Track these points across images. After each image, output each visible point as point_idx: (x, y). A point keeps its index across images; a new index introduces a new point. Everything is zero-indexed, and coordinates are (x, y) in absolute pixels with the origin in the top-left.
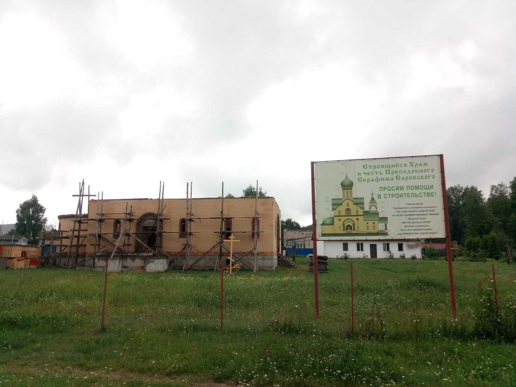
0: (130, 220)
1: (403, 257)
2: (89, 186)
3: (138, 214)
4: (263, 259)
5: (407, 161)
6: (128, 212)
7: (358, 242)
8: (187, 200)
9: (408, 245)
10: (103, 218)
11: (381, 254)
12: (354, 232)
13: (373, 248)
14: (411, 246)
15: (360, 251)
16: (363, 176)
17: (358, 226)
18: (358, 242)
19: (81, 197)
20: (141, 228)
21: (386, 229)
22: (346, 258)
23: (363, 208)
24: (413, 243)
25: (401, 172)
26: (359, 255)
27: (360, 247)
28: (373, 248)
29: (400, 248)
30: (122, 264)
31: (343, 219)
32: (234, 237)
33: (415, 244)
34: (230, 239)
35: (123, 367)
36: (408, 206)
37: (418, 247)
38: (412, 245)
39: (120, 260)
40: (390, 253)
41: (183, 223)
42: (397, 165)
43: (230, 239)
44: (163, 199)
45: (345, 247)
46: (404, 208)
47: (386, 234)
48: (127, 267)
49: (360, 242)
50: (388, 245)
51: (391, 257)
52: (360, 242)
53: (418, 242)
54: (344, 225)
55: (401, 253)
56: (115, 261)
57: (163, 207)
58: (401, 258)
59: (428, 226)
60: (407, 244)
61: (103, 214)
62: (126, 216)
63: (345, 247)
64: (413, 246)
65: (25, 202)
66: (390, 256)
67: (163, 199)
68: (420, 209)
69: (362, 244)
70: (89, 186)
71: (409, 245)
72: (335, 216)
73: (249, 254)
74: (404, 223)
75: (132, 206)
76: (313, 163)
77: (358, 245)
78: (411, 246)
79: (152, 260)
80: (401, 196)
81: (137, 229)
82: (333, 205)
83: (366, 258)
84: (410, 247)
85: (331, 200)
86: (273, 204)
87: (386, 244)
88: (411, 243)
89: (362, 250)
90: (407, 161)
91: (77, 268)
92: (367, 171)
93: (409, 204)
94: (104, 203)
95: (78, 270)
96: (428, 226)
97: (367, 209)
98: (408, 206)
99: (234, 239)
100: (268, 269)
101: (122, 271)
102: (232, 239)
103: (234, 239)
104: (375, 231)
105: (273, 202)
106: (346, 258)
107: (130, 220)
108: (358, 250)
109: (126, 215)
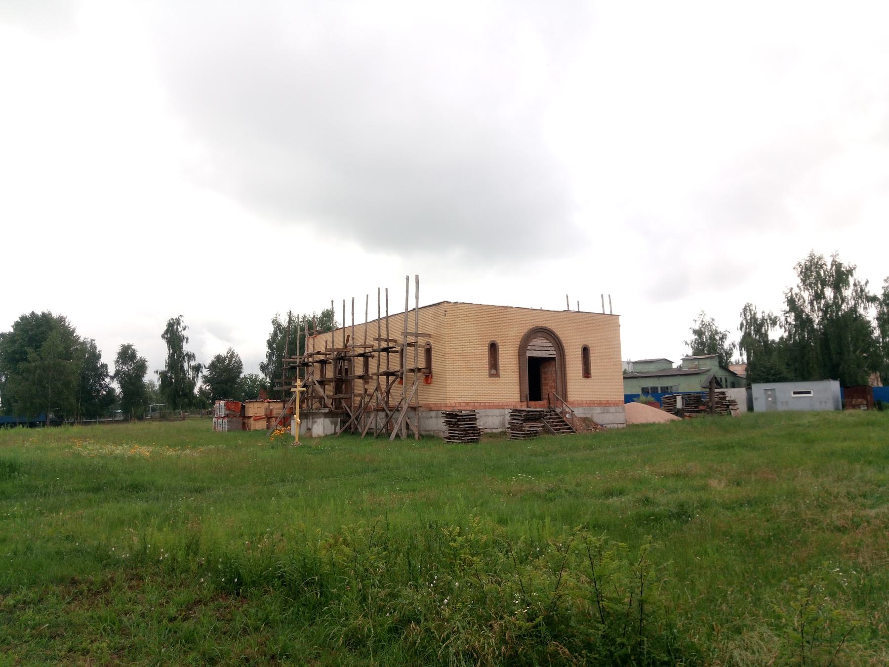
67: (353, 326)
109: (380, 352)
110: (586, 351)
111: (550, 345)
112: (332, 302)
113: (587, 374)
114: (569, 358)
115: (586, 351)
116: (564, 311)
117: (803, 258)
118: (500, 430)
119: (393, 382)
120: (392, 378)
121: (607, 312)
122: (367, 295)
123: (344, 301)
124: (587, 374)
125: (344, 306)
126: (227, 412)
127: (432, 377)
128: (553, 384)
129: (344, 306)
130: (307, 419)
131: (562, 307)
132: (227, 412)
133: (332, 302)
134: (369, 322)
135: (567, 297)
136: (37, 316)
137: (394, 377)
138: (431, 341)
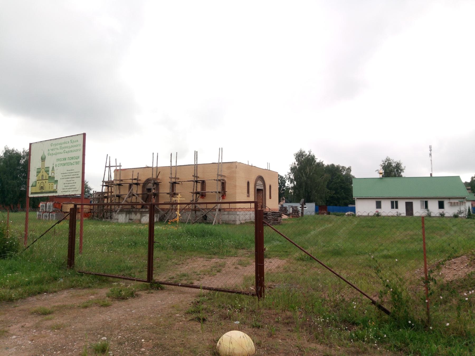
0: (137, 184)
1: (442, 215)
2: (116, 159)
3: (143, 179)
4: (228, 214)
5: (68, 140)
6: (173, 176)
7: (393, 200)
8: (219, 164)
9: (450, 202)
10: (121, 182)
11: (418, 210)
12: (44, 191)
13: (409, 207)
14: (453, 204)
15: (395, 209)
16: (51, 152)
17: (45, 187)
18: (393, 200)
19: (196, 163)
20: (145, 190)
21: (57, 189)
22: (378, 215)
23: (48, 174)
24: (456, 201)
25: (66, 147)
26: (394, 212)
27: (394, 205)
28: (409, 207)
29: (441, 205)
30: (129, 217)
31: (40, 182)
32: (181, 196)
33: (459, 201)
34: (178, 198)
35: (104, 281)
36: (68, 172)
37: (463, 205)
38: (454, 203)
39: (126, 214)
40: (428, 211)
41: (173, 184)
42: (65, 143)
43: (178, 198)
44: (157, 167)
45: (379, 205)
46: (65, 173)
47: (56, 192)
48: (132, 220)
49: (394, 200)
50: (426, 203)
51: (429, 215)
52: (394, 200)
53: (462, 200)
54: (40, 186)
55: (441, 211)
56: (123, 215)
57: (158, 173)
58: (440, 216)
59: (75, 186)
60: (449, 201)
61: (121, 180)
62: (132, 181)
63: (379, 205)
64: (456, 204)
65: (333, 165)
66: (428, 214)
67: (157, 167)
68: (73, 174)
69: (397, 202)
70: (116, 159)
71: (451, 203)
72: (37, 180)
73: (212, 210)
74: (64, 184)
75: (138, 173)
76: (31, 144)
77: (392, 203)
78: (453, 204)
79: (144, 214)
80: (65, 164)
81: (143, 191)
82: (37, 172)
83: (399, 216)
84: (452, 205)
85: (36, 169)
86: (236, 168)
87: (424, 201)
88: (452, 201)
89: (397, 207)
90: (68, 140)
91: (104, 220)
92: (52, 147)
93: (68, 171)
94: (122, 172)
95: (104, 222)
96: (75, 186)
97: (50, 175)
98: (68, 172)
99: (180, 197)
100: (232, 223)
101: (129, 222)
102: (179, 198)
103: (180, 197)
104: (52, 190)
105: (236, 166)
106: (378, 215)
107: (137, 184)
108: (392, 207)
109: (132, 180)
110: (270, 186)
111: (262, 184)
112: (153, 153)
113: (270, 198)
114: (267, 190)
115: (270, 186)
116: (265, 169)
117: (297, 151)
118: (249, 221)
119: (199, 197)
120: (198, 195)
121: (269, 169)
122: (177, 153)
123: (158, 153)
124: (270, 198)
125: (157, 156)
126: (54, 209)
127: (225, 196)
128: (261, 201)
129: (157, 156)
130: (129, 214)
131: (265, 167)
132: (54, 209)
133: (153, 153)
134: (172, 166)
135: (171, 155)
136: (323, 165)
137: (199, 195)
138: (226, 179)
